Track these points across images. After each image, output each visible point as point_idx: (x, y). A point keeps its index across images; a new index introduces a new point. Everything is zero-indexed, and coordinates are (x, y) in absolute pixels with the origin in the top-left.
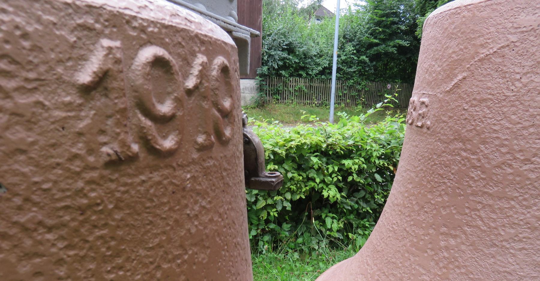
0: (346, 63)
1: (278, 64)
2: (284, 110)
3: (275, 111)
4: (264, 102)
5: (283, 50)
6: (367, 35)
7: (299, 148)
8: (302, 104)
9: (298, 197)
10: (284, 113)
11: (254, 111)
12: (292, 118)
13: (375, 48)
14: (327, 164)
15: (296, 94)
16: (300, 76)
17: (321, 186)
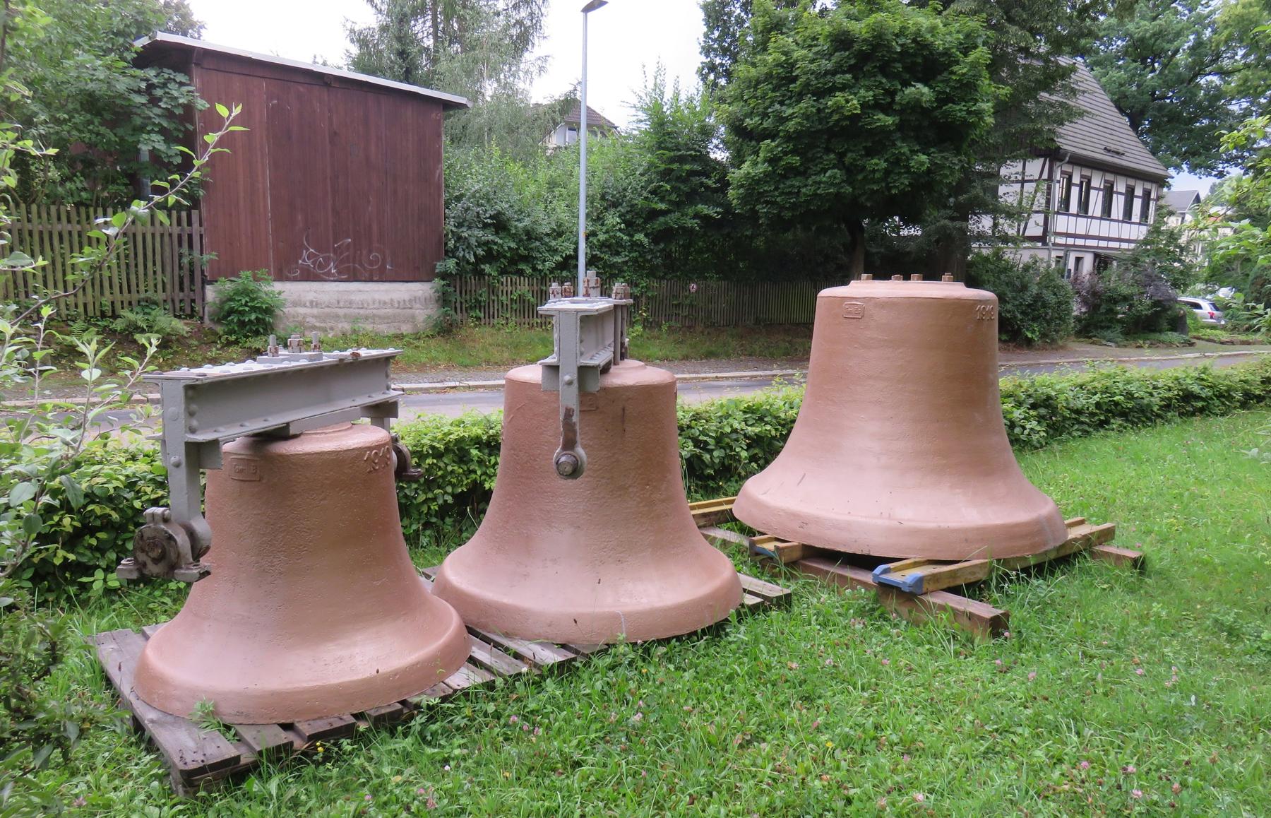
0: (609, 247)
1: (475, 255)
2: (490, 340)
3: (474, 341)
4: (451, 325)
5: (485, 226)
6: (645, 194)
7: (460, 440)
8: (527, 326)
9: (460, 490)
10: (490, 345)
11: (432, 342)
12: (506, 355)
13: (662, 219)
14: (490, 455)
15: (515, 306)
16: (521, 273)
17: (483, 478)
